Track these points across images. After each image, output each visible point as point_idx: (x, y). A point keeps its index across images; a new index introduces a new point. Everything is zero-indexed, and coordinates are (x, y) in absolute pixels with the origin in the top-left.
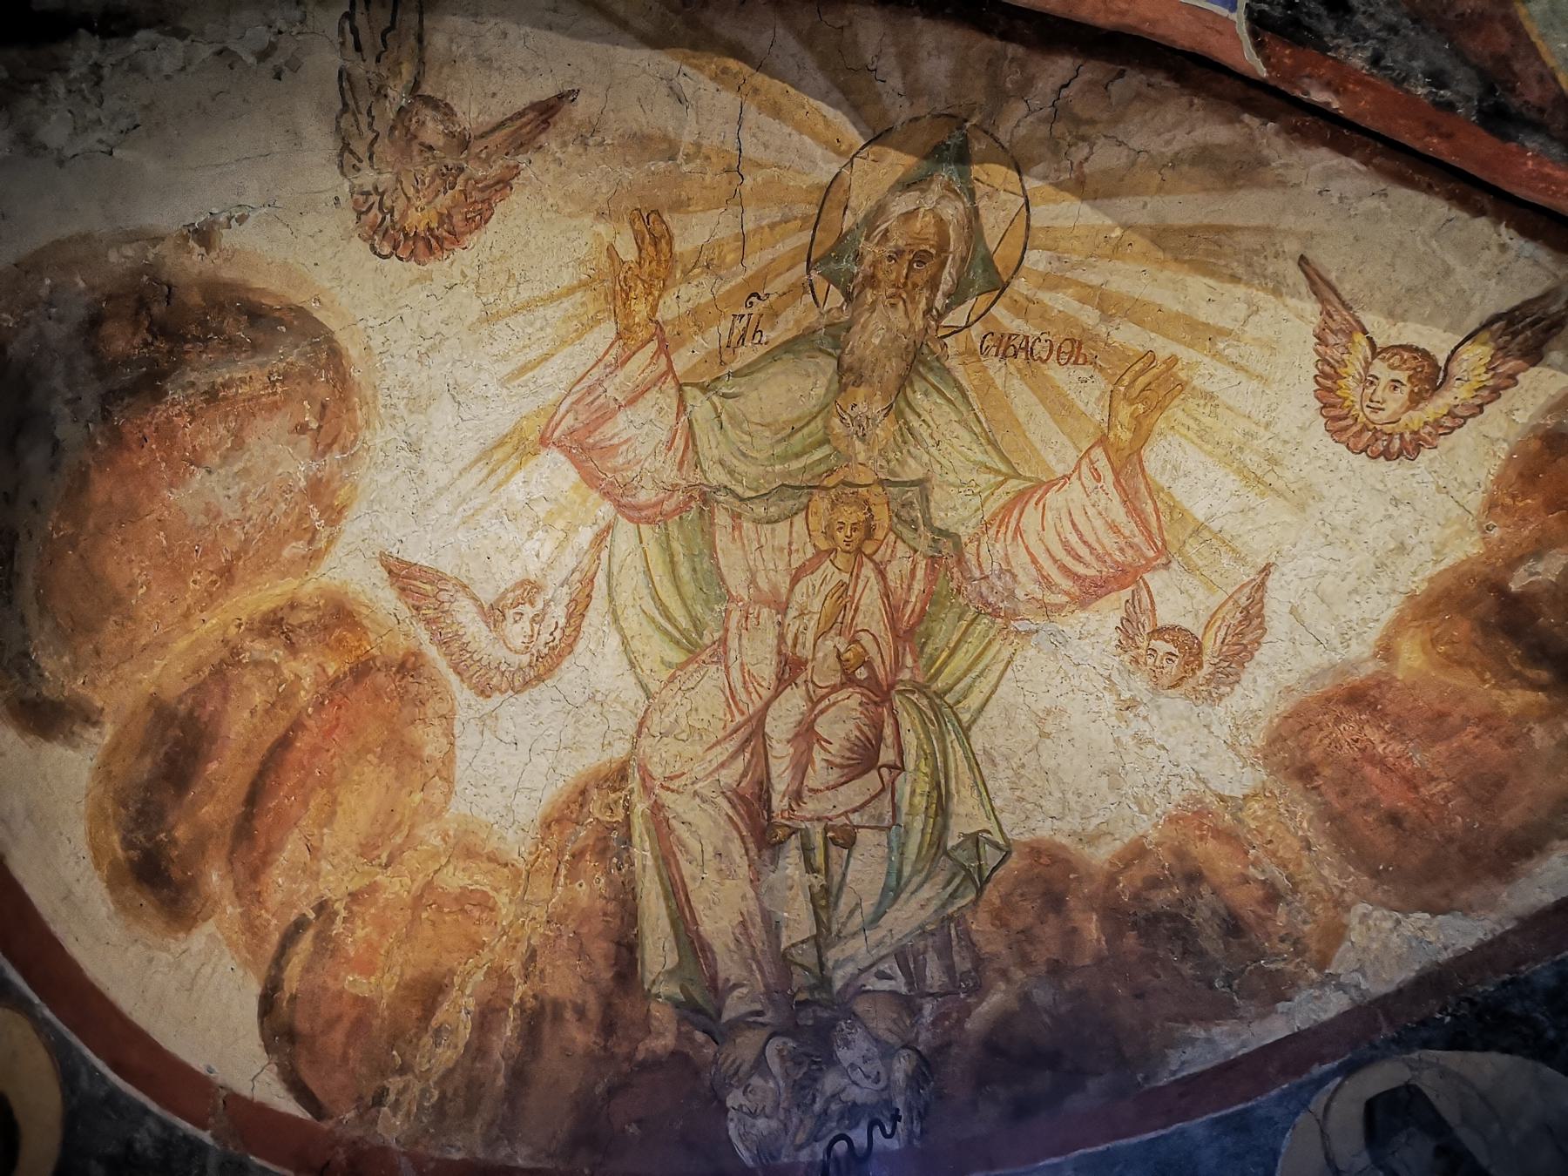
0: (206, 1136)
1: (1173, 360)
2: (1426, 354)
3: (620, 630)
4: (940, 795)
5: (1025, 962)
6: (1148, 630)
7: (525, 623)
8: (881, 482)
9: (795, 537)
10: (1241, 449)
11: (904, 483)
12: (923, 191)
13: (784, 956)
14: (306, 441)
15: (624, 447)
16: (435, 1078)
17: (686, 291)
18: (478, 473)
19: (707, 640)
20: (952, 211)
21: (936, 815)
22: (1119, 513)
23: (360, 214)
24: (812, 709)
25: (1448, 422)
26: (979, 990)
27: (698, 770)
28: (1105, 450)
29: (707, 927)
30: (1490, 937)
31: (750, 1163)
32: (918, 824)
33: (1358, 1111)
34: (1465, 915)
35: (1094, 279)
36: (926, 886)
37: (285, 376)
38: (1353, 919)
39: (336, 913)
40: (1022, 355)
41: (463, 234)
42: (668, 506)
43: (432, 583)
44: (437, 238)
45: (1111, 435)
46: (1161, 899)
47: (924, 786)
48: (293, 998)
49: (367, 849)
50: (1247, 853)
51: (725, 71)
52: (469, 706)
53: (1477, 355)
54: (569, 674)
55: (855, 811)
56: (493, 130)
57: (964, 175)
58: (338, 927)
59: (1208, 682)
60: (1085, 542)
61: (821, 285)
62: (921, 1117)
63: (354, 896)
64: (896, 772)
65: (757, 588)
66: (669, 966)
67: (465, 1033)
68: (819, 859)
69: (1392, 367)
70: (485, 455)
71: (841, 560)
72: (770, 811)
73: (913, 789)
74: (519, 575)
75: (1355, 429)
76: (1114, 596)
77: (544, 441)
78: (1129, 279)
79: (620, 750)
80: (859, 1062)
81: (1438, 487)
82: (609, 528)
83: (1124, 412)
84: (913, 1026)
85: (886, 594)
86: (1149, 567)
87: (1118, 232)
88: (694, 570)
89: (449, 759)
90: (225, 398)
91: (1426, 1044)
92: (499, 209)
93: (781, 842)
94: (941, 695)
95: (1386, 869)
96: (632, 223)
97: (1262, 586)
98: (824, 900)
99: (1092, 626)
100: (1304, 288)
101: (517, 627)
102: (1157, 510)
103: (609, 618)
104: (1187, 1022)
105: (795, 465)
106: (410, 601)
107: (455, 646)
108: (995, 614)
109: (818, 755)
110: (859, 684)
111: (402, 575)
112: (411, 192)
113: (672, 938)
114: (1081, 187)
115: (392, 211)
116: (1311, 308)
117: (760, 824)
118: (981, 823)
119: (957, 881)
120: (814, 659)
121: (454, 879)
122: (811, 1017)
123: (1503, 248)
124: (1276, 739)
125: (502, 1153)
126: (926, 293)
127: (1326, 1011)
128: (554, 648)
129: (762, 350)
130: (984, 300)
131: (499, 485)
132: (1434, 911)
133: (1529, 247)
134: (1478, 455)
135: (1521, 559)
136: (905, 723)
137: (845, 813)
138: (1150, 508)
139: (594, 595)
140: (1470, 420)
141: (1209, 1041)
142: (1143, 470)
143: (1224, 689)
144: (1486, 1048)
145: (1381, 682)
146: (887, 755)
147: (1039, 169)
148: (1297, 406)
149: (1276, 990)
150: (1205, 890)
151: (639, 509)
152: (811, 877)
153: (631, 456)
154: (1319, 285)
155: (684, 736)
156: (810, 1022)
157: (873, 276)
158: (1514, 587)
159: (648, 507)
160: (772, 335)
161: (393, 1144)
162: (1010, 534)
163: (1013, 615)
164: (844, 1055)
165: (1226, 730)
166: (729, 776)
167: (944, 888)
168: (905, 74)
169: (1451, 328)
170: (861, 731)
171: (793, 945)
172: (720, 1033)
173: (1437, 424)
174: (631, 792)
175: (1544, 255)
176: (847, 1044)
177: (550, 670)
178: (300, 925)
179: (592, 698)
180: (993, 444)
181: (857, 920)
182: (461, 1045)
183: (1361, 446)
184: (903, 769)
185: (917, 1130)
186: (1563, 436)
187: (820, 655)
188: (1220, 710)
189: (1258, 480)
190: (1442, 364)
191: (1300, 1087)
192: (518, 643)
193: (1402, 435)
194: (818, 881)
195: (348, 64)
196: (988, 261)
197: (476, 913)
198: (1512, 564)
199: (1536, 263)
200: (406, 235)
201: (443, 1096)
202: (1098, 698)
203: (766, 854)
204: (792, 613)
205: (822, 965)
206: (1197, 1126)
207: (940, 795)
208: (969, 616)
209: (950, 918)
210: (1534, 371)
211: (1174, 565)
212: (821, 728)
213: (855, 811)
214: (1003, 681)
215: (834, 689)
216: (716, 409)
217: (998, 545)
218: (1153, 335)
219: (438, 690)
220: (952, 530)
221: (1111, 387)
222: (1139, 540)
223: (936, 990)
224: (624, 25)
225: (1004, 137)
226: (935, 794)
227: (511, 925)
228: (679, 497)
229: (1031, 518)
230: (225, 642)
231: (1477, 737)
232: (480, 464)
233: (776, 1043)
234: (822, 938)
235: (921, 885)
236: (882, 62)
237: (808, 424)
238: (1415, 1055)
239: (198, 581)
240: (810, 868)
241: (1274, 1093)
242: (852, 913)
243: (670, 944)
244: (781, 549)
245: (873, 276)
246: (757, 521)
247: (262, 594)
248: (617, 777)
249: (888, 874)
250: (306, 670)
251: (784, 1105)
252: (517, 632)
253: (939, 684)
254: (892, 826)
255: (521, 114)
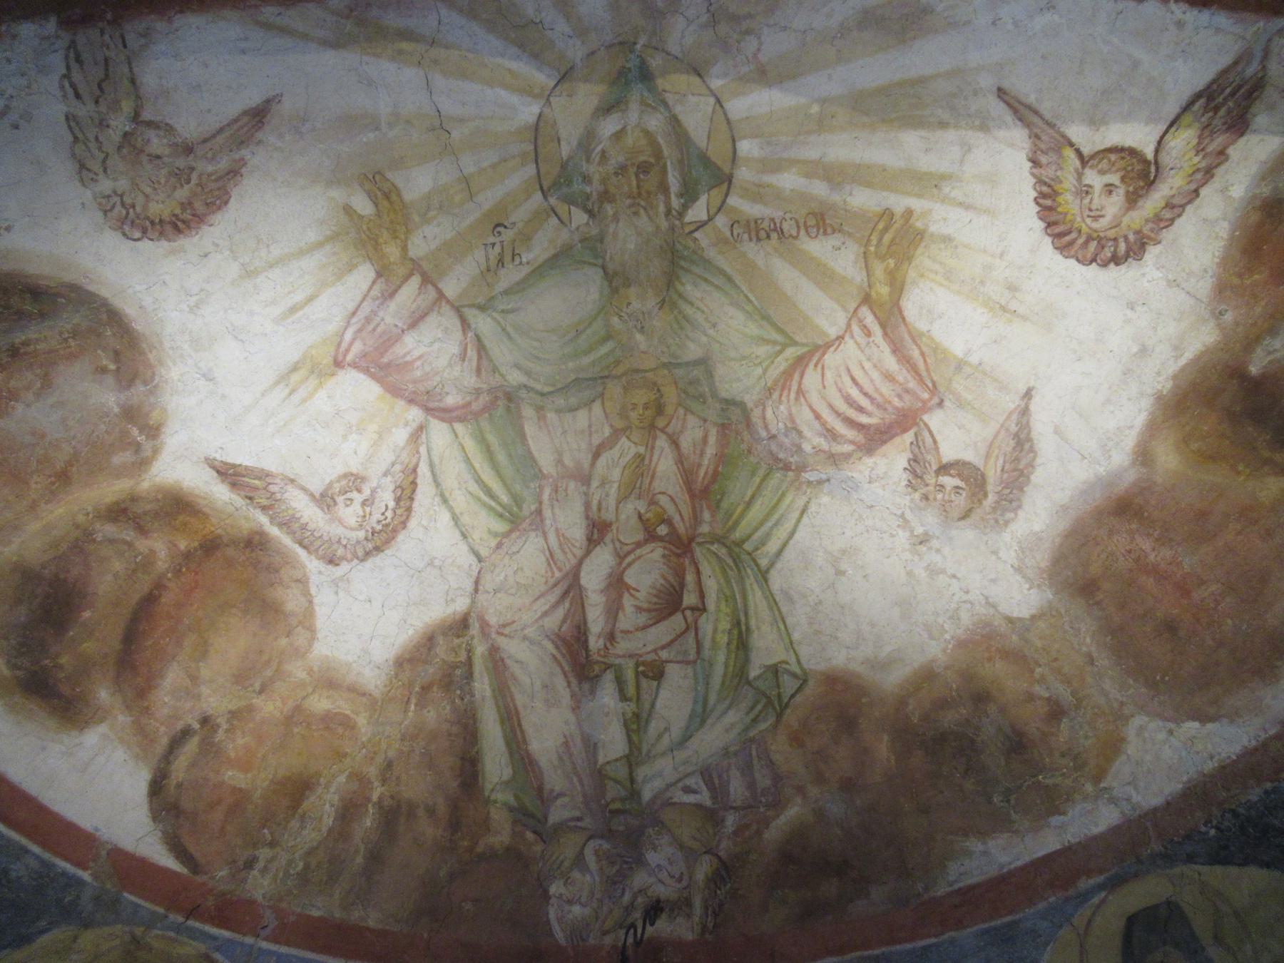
0: (86, 876)
1: (909, 213)
2: (1132, 152)
3: (451, 509)
4: (740, 633)
5: (820, 779)
6: (935, 467)
7: (356, 506)
8: (665, 365)
9: (591, 421)
10: (982, 282)
11: (687, 364)
12: (624, 111)
13: (600, 772)
14: (110, 380)
15: (419, 363)
16: (301, 852)
17: (430, 230)
18: (281, 392)
19: (526, 512)
20: (655, 122)
21: (738, 648)
22: (891, 363)
23: (105, 212)
24: (620, 564)
25: (1167, 214)
26: (778, 805)
27: (527, 617)
28: (871, 309)
29: (535, 746)
30: (1254, 743)
31: (563, 942)
32: (721, 658)
33: (1118, 925)
34: (1232, 721)
35: (813, 154)
36: (731, 713)
37: (75, 334)
38: (1130, 731)
39: (218, 726)
40: (774, 235)
41: (205, 215)
42: (476, 406)
43: (260, 479)
44: (184, 222)
45: (873, 293)
46: (949, 719)
47: (725, 625)
48: (179, 785)
49: (241, 678)
50: (1032, 671)
51: (400, 52)
52: (320, 572)
53: (1182, 141)
54: (407, 546)
55: (663, 648)
56: (214, 136)
57: (652, 89)
58: (220, 735)
59: (994, 509)
60: (866, 394)
61: (562, 209)
62: (716, 915)
63: (234, 715)
64: (697, 613)
65: (563, 465)
66: (505, 777)
67: (328, 821)
68: (631, 690)
69: (1102, 172)
70: (283, 378)
71: (636, 436)
72: (587, 649)
73: (715, 626)
74: (340, 469)
75: (1080, 241)
76: (898, 440)
77: (338, 364)
78: (844, 148)
79: (461, 605)
80: (664, 863)
81: (1168, 281)
82: (421, 428)
83: (879, 269)
84: (715, 834)
85: (680, 461)
86: (925, 408)
87: (815, 109)
88: (510, 456)
89: (309, 612)
90: (25, 353)
91: (1190, 859)
92: (235, 193)
93: (597, 676)
94: (739, 544)
95: (1163, 678)
96: (361, 185)
97: (1025, 412)
98: (635, 724)
99: (881, 469)
100: (1009, 117)
101: (350, 510)
102: (923, 354)
103: (438, 499)
104: (966, 835)
105: (586, 360)
106: (243, 493)
107: (296, 526)
108: (787, 467)
109: (628, 602)
110: (661, 539)
111: (230, 474)
112: (148, 190)
113: (507, 755)
114: (763, 75)
115: (133, 206)
116: (1019, 135)
117: (579, 659)
118: (779, 654)
119: (759, 707)
120: (617, 520)
121: (320, 704)
122: (624, 822)
123: (1180, 24)
124: (1059, 560)
125: (356, 915)
126: (662, 197)
127: (1097, 826)
128: (387, 525)
129: (526, 270)
130: (717, 194)
131: (304, 401)
132: (1204, 718)
133: (1204, 16)
134: (1199, 242)
135: (1258, 339)
136: (706, 569)
137: (655, 651)
138: (916, 354)
139: (419, 481)
140: (1189, 207)
141: (985, 853)
142: (904, 319)
143: (1009, 515)
144: (1245, 863)
145: (1143, 488)
146: (689, 599)
147: (716, 69)
148: (1026, 228)
149: (1052, 802)
150: (992, 709)
151: (444, 410)
152: (624, 704)
153: (428, 369)
154: (1021, 111)
155: (513, 591)
156: (621, 828)
157: (606, 192)
158: (1254, 370)
159: (457, 408)
160: (531, 256)
161: (260, 899)
162: (793, 395)
163: (801, 468)
164: (653, 858)
165: (1013, 554)
166: (552, 622)
167: (748, 713)
168: (568, 17)
169: (1151, 120)
170: (665, 579)
171: (608, 763)
172: (548, 835)
173: (1157, 219)
174: (472, 638)
175: (1222, 19)
176: (655, 849)
177: (387, 542)
178: (186, 733)
179: (431, 564)
180: (767, 318)
181: (666, 741)
182: (325, 829)
183: (1089, 256)
184: (704, 610)
185: (710, 925)
186: (1280, 201)
187: (623, 517)
188: (1007, 536)
189: (1004, 309)
190: (1150, 156)
191: (1067, 900)
192: (353, 522)
193: (1126, 238)
194: (630, 708)
195: (72, 110)
196: (705, 160)
197: (340, 730)
198: (1250, 343)
199: (1218, 30)
200: (152, 223)
201: (307, 867)
202: (892, 536)
203: (586, 686)
204: (595, 484)
205: (632, 780)
206: (967, 935)
207: (740, 633)
208: (761, 473)
209: (752, 740)
210: (1242, 141)
211: (947, 403)
212: (630, 578)
213: (663, 648)
214: (801, 527)
215: (639, 545)
216: (499, 323)
217: (782, 408)
218: (885, 194)
219: (289, 560)
220: (738, 399)
221: (862, 249)
222: (912, 384)
223: (739, 803)
224: (305, 37)
225: (674, 48)
226: (736, 632)
227: (369, 741)
228: (485, 398)
229: (811, 379)
230: (77, 526)
231: (1239, 533)
232: (282, 385)
233: (592, 844)
234: (632, 759)
235: (725, 712)
236: (544, 14)
237: (590, 324)
238: (1177, 870)
239: (37, 484)
240: (624, 697)
241: (1041, 906)
242: (660, 736)
243: (505, 759)
244: (583, 431)
245: (606, 192)
246: (559, 411)
247: (110, 490)
248: (460, 625)
249: (695, 702)
250: (160, 548)
251: (598, 896)
252: (350, 513)
253: (737, 535)
254: (697, 660)
255: (236, 121)
